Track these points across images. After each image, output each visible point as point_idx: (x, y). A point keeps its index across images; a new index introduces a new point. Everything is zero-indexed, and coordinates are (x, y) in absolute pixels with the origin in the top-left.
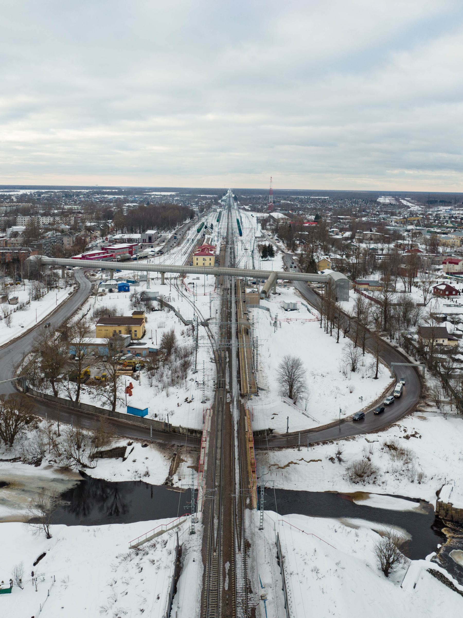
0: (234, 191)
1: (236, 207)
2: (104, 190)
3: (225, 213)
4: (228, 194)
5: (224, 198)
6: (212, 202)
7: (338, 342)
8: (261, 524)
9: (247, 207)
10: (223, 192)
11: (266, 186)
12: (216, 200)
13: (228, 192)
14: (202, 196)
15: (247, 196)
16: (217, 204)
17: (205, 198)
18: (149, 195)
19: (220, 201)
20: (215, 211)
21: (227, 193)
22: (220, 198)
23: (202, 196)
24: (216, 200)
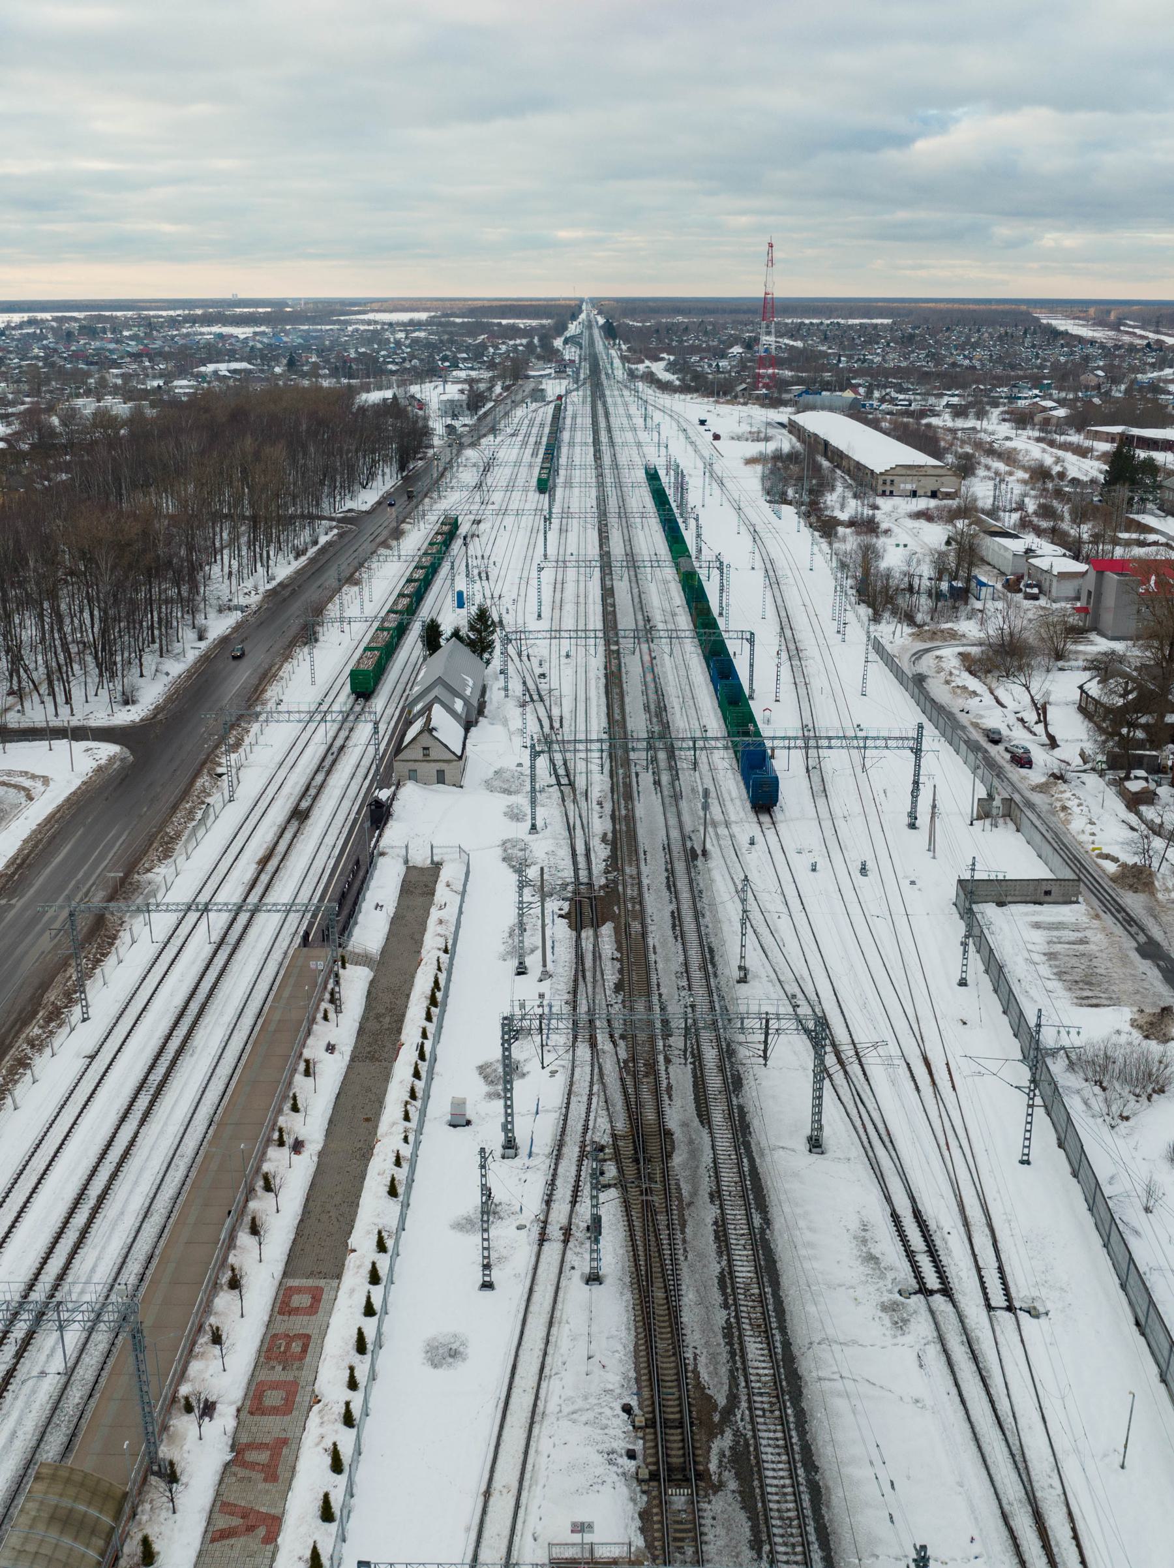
0: (599, 305)
1: (620, 373)
2: (238, 310)
3: (578, 404)
4: (583, 316)
5: (573, 328)
6: (530, 346)
7: (934, 858)
8: (595, 1264)
9: (659, 369)
10: (563, 313)
11: (742, 283)
12: (546, 337)
13: (584, 307)
14: (504, 322)
15: (643, 321)
16: (550, 354)
17: (514, 332)
18: (339, 322)
19: (558, 343)
20: (538, 395)
21: (581, 311)
22: (561, 328)
23: (504, 322)
24: (546, 337)
